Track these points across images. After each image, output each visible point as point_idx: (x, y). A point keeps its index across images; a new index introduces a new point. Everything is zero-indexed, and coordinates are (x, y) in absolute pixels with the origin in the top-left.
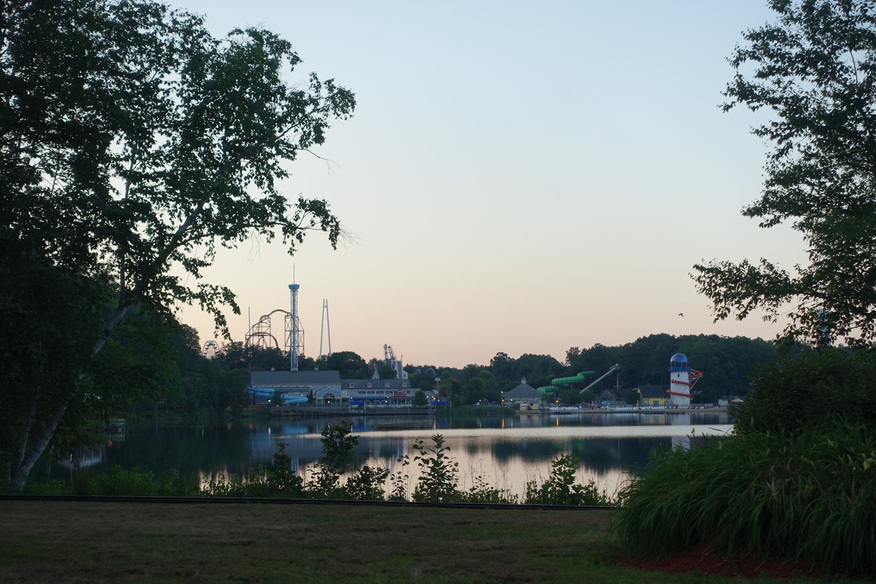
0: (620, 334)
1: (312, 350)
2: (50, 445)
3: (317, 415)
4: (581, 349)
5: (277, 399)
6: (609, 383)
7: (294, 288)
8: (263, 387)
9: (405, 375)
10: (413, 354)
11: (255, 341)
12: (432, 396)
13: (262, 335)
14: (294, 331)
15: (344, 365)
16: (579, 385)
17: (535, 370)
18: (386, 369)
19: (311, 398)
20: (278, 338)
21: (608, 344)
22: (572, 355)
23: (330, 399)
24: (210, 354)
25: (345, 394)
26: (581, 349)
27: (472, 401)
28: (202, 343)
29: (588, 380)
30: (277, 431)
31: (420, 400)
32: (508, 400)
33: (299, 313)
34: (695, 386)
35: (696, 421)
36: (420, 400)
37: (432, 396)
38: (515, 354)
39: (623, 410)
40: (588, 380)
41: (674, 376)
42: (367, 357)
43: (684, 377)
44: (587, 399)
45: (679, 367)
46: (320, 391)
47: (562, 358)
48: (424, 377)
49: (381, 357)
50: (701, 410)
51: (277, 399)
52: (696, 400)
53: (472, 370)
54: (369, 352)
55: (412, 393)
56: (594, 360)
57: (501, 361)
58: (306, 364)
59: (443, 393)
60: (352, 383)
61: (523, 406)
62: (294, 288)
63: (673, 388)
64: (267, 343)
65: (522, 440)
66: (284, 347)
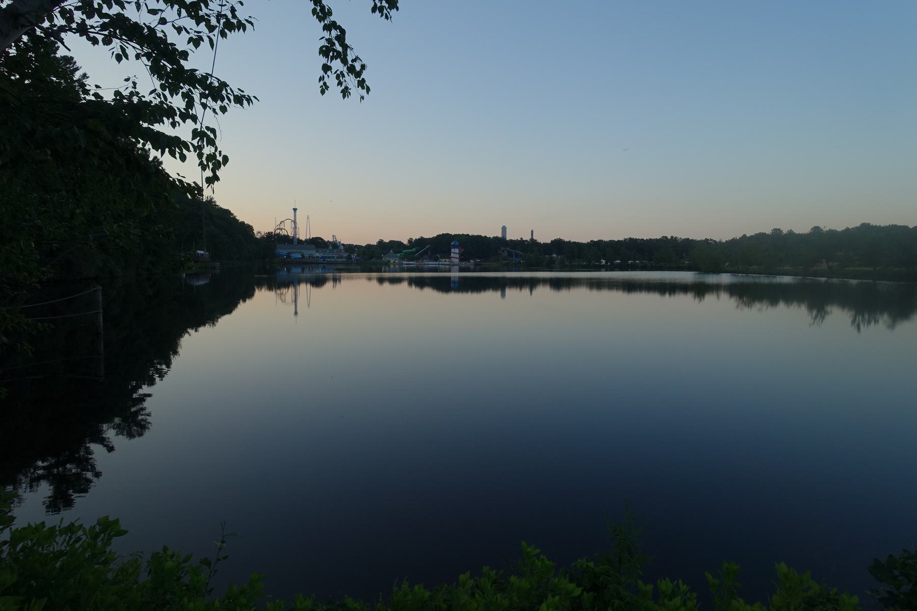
0: (430, 234)
1: (303, 237)
2: (816, 274)
3: (306, 263)
4: (93, 456)
5: (289, 255)
6: (425, 253)
7: (295, 210)
8: (283, 251)
9: (342, 247)
10: (346, 239)
11: (278, 231)
12: (354, 256)
14: (295, 228)
15: (317, 243)
16: (413, 253)
17: (396, 246)
18: (335, 245)
20: (288, 231)
21: (426, 236)
22: (410, 241)
23: (311, 257)
24: (258, 236)
25: (317, 254)
26: (93, 456)
27: (371, 258)
28: (255, 232)
29: (417, 251)
30: (289, 270)
31: (349, 258)
32: (385, 259)
33: (297, 221)
34: (461, 254)
35: (461, 270)
36: (349, 258)
37: (354, 256)
38: (387, 240)
39: (432, 264)
40: (417, 251)
41: (453, 250)
42: (326, 239)
43: (457, 251)
44: (417, 259)
45: (455, 247)
46: (307, 253)
47: (405, 242)
48: (350, 248)
49: (331, 240)
50: (464, 264)
51: (289, 255)
52: (461, 260)
53: (369, 246)
54: (327, 238)
55: (346, 255)
56: (421, 243)
57: (381, 242)
58: (300, 242)
59: (358, 255)
60: (320, 250)
61: (392, 261)
62: (295, 210)
63: (452, 255)
64: (283, 233)
65: (668, 281)
66: (291, 234)
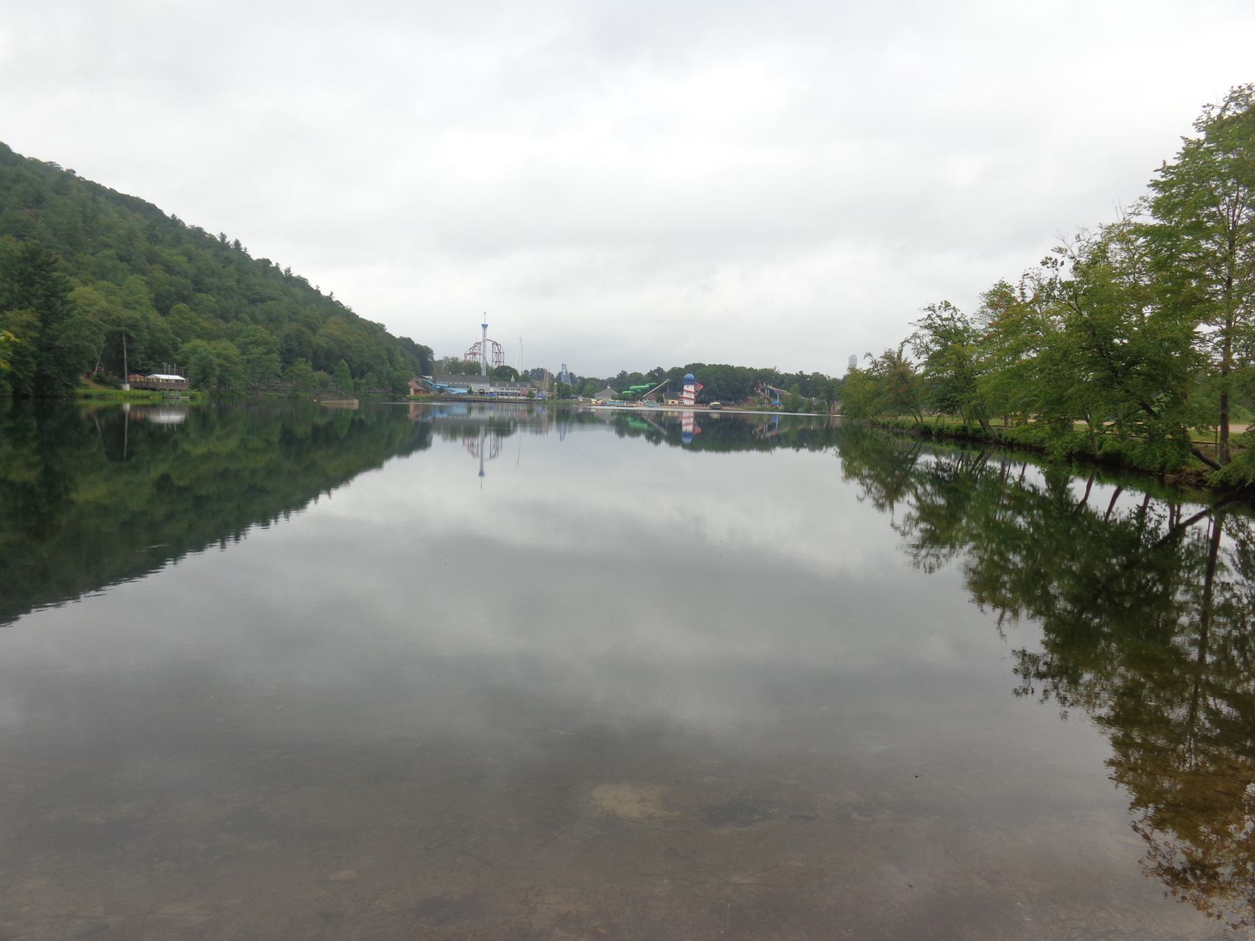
13: (475, 354)
19: (470, 392)
25: (492, 390)
41: (685, 388)
43: (691, 388)
45: (690, 382)
